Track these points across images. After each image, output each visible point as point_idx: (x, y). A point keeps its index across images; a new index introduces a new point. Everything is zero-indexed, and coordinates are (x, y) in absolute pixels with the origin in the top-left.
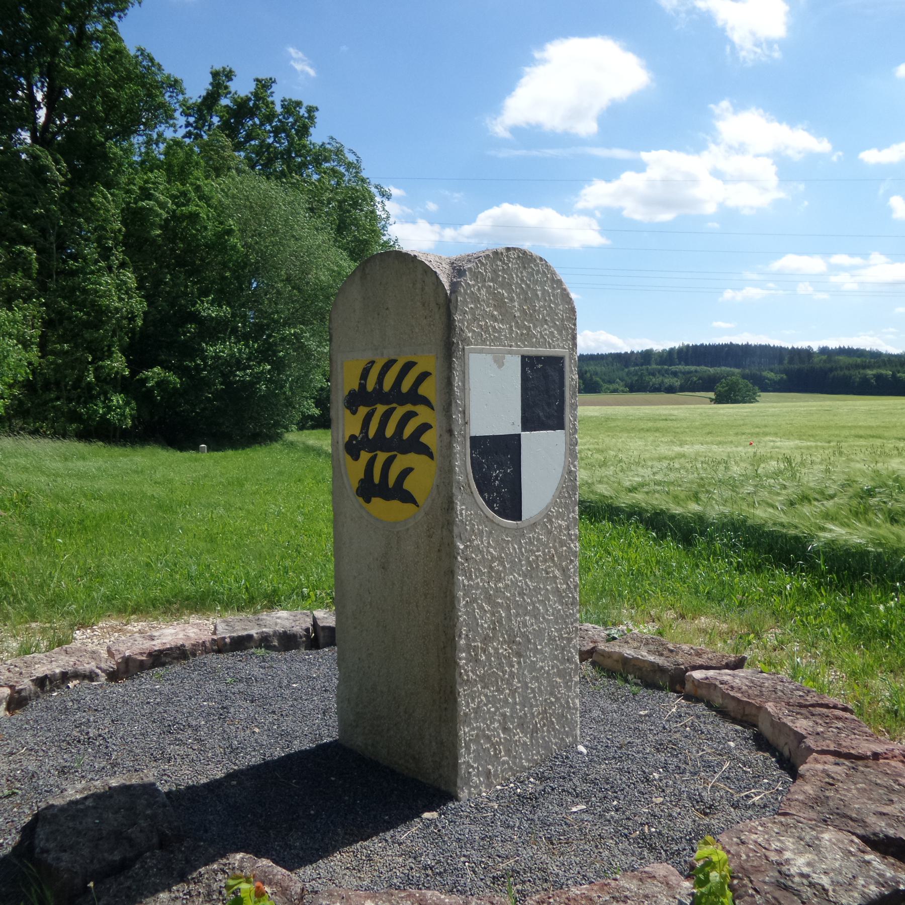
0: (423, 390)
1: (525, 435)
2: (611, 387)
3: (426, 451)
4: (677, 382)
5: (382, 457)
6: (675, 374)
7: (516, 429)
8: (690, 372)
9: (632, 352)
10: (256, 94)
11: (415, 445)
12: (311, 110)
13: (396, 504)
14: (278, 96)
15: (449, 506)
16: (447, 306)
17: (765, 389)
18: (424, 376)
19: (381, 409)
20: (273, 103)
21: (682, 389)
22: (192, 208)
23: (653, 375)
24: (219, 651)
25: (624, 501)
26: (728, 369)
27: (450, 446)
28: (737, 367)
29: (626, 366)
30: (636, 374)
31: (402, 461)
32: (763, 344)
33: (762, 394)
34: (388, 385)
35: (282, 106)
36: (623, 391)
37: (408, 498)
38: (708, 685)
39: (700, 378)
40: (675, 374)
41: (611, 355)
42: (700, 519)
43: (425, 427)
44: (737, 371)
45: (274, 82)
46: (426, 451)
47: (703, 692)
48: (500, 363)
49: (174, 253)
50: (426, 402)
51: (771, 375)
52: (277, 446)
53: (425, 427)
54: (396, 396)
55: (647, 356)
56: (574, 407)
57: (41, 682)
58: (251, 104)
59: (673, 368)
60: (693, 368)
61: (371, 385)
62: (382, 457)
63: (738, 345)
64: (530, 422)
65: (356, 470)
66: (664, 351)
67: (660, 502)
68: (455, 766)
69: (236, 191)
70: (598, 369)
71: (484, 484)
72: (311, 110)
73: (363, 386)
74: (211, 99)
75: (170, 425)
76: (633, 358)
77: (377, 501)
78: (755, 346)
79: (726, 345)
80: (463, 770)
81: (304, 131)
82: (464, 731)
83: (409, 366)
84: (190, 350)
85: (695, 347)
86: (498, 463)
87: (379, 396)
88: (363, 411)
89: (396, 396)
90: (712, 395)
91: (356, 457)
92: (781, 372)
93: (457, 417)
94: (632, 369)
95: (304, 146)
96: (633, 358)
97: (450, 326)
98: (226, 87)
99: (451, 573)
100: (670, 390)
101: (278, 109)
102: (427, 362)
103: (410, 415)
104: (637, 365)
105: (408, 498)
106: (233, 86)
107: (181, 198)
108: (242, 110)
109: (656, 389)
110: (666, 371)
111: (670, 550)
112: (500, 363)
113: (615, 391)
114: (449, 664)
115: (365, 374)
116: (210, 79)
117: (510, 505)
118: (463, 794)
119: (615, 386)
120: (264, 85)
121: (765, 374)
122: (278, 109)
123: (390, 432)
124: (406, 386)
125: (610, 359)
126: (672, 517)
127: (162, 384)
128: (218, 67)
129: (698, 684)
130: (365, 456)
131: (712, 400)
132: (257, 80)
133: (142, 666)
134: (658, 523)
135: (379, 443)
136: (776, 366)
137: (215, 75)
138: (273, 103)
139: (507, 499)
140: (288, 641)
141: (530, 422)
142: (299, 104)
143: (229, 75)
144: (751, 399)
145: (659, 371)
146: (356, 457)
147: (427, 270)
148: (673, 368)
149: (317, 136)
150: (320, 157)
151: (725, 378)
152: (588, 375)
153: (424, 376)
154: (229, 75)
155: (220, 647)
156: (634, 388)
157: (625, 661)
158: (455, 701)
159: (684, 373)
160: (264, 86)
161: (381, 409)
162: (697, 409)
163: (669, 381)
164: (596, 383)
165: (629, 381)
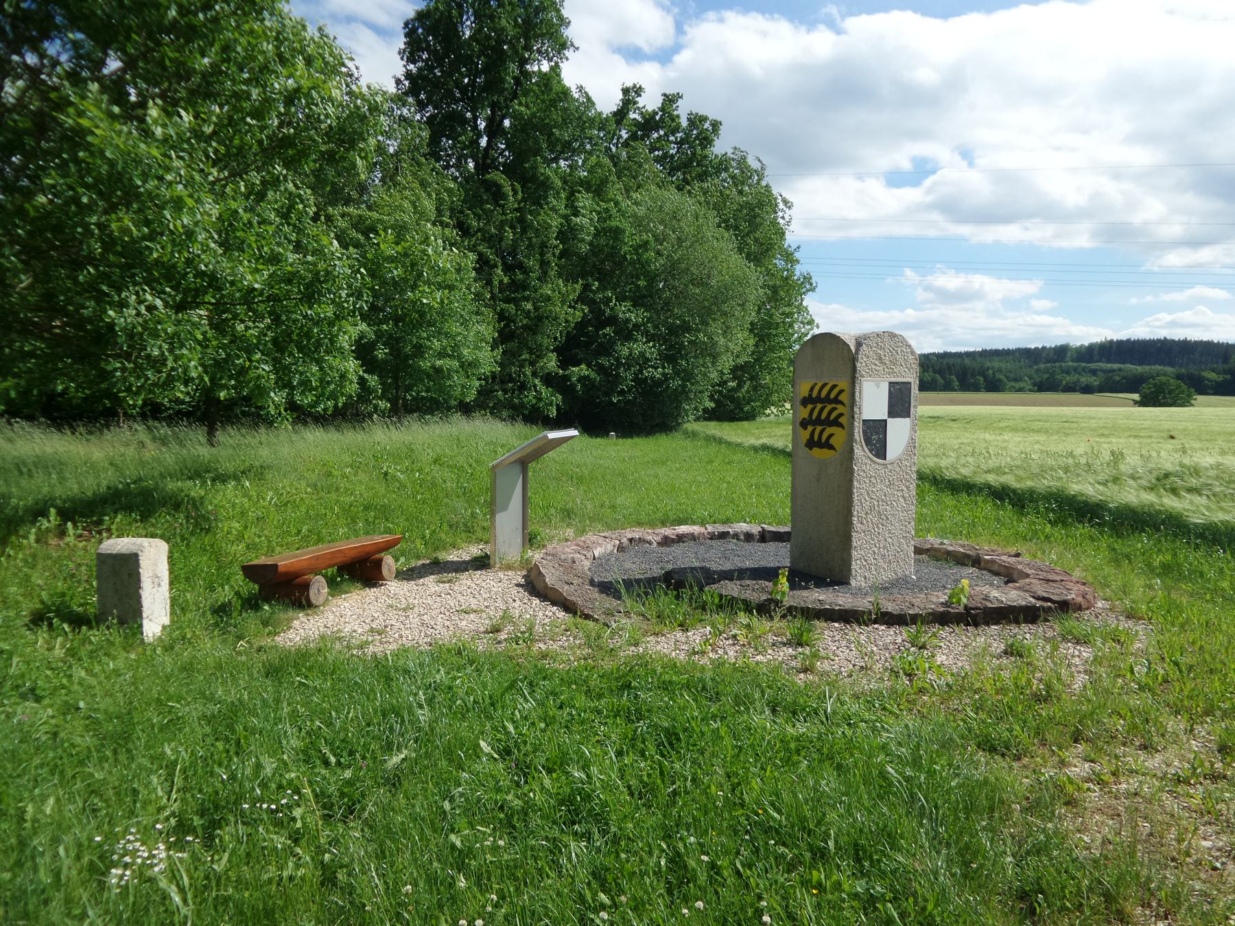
0: (841, 398)
1: (889, 420)
2: (1017, 385)
3: (841, 426)
4: (1094, 381)
5: (819, 428)
6: (1094, 372)
7: (885, 417)
8: (1112, 371)
9: (1044, 348)
10: (662, 109)
11: (836, 423)
12: (716, 125)
13: (825, 450)
14: (683, 111)
15: (852, 451)
16: (853, 360)
17: (1203, 391)
18: (842, 391)
19: (819, 406)
20: (678, 116)
21: (1101, 389)
22: (614, 223)
23: (1068, 373)
24: (711, 539)
25: (980, 479)
26: (1159, 367)
27: (852, 424)
28: (1171, 365)
29: (1036, 363)
30: (1047, 372)
31: (829, 431)
32: (1205, 339)
33: (1199, 397)
34: (823, 394)
35: (689, 119)
36: (1030, 391)
37: (831, 447)
38: (993, 561)
39: (1124, 378)
40: (1094, 372)
41: (1019, 350)
42: (1032, 492)
43: (841, 415)
44: (1169, 369)
45: (681, 97)
46: (841, 426)
47: (989, 565)
48: (878, 386)
49: (604, 264)
50: (841, 403)
51: (1213, 376)
52: (677, 435)
53: (841, 415)
54: (827, 400)
55: (1061, 352)
56: (915, 407)
57: (631, 540)
58: (657, 118)
59: (1093, 366)
60: (1116, 366)
61: (814, 395)
62: (819, 428)
63: (1173, 341)
64: (893, 413)
65: (805, 435)
66: (1081, 346)
67: (1010, 480)
68: (850, 570)
69: (651, 207)
70: (1003, 366)
71: (868, 441)
72: (716, 125)
73: (810, 395)
74: (620, 115)
75: (595, 414)
76: (1044, 355)
77: (816, 450)
78: (1196, 342)
79: (1159, 341)
80: (853, 573)
81: (706, 141)
82: (854, 553)
83: (834, 386)
84: (606, 349)
85: (1120, 343)
86: (876, 434)
87: (819, 400)
88: (810, 407)
89: (827, 400)
90: (1136, 396)
91: (805, 428)
92: (1225, 372)
93: (856, 410)
94: (1042, 366)
95: (706, 157)
96: (1044, 355)
97: (854, 369)
98: (635, 103)
99: (851, 481)
100: (1087, 390)
101: (684, 123)
102: (843, 384)
103: (834, 409)
104: (1049, 362)
105: (831, 447)
106: (641, 101)
107: (605, 216)
108: (649, 123)
109: (1069, 389)
110: (1084, 368)
111: (1007, 513)
112: (878, 386)
113: (1020, 390)
114: (848, 525)
115: (812, 389)
116: (621, 96)
117: (881, 452)
118: (853, 582)
119: (1021, 384)
120: (670, 100)
121: (1204, 374)
122: (684, 123)
123: (824, 416)
124: (832, 396)
125: (1017, 354)
126: (1014, 491)
127: (582, 379)
128: (629, 84)
129: (988, 561)
130: (810, 428)
131: (1136, 403)
132: (665, 95)
133: (673, 541)
134: (1000, 494)
135: (818, 421)
136: (1220, 366)
137: (626, 91)
138: (678, 116)
139: (879, 450)
140: (749, 537)
141: (893, 413)
142: (703, 119)
143: (638, 91)
144: (1186, 403)
145: (1075, 369)
146: (805, 428)
147: (844, 343)
148: (1093, 366)
149: (721, 147)
150: (722, 165)
151: (1153, 377)
152: (991, 372)
153: (842, 391)
154: (638, 91)
155: (713, 537)
156: (1042, 387)
157: (948, 553)
158: (851, 541)
159: (1104, 371)
160: (670, 101)
161: (819, 406)
162: (1121, 412)
163: (1085, 380)
164: (1000, 380)
165: (1038, 379)
